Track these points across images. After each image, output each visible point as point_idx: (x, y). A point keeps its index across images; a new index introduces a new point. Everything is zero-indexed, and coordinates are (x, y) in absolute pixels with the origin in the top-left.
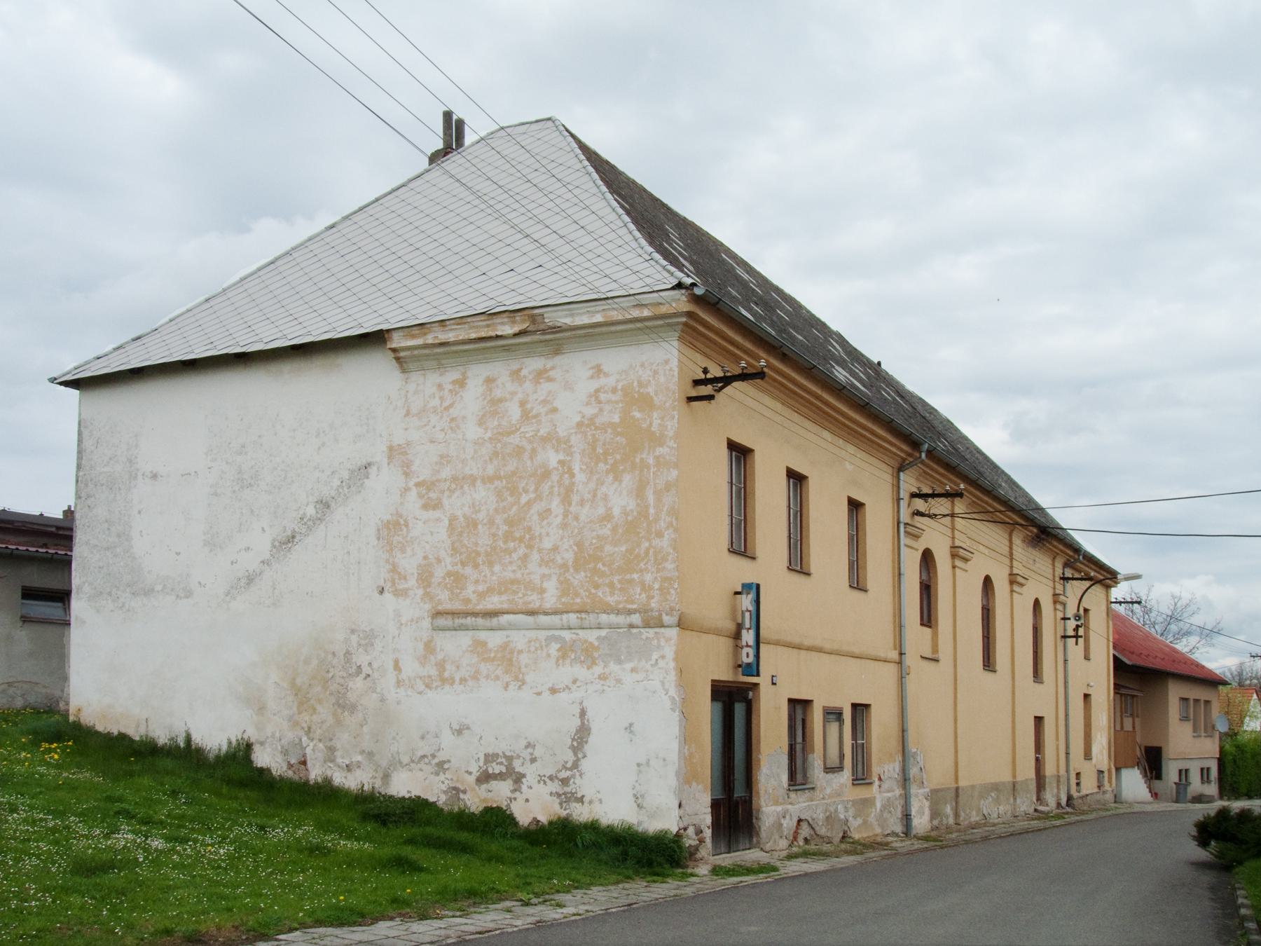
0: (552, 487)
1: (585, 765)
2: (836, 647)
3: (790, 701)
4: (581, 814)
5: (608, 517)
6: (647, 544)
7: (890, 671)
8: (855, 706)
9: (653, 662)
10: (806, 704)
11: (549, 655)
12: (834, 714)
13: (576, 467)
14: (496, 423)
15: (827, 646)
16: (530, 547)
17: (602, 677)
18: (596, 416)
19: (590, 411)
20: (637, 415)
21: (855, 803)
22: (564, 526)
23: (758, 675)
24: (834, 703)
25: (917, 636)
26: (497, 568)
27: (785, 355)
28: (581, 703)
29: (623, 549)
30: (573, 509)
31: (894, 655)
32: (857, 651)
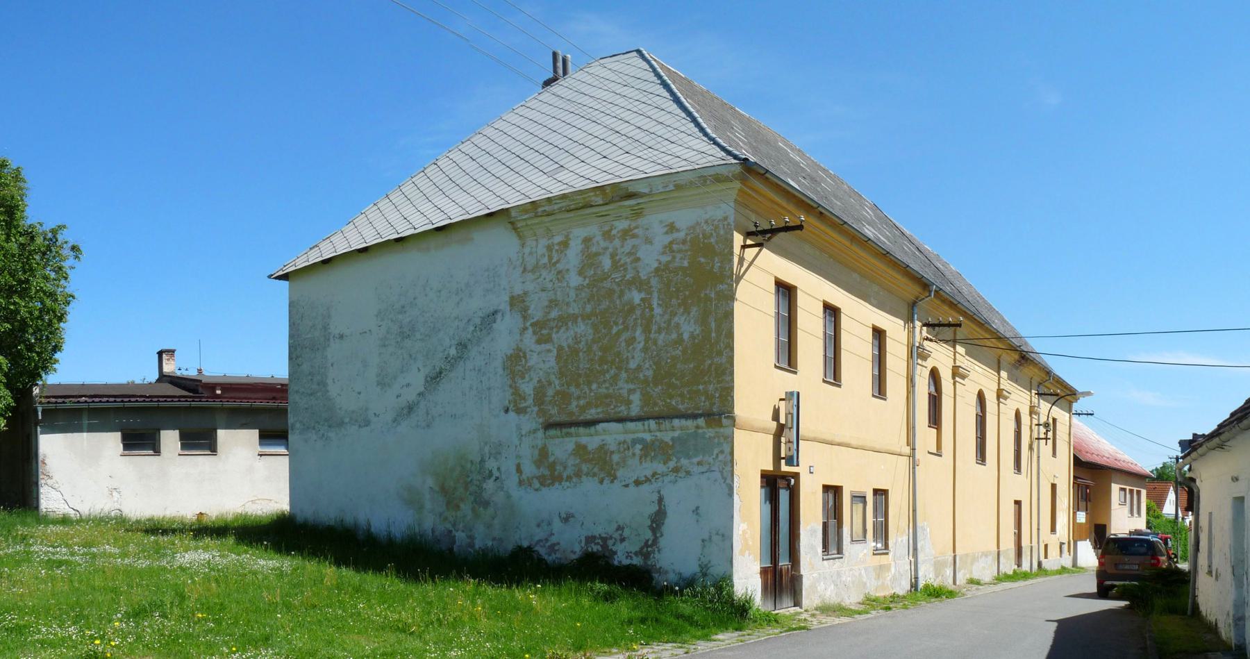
1: (662, 542)
2: (861, 443)
11: (634, 454)
13: (655, 303)
15: (854, 443)
17: (676, 470)
18: (669, 262)
25: (926, 436)
26: (594, 386)
31: (907, 450)
32: (878, 447)
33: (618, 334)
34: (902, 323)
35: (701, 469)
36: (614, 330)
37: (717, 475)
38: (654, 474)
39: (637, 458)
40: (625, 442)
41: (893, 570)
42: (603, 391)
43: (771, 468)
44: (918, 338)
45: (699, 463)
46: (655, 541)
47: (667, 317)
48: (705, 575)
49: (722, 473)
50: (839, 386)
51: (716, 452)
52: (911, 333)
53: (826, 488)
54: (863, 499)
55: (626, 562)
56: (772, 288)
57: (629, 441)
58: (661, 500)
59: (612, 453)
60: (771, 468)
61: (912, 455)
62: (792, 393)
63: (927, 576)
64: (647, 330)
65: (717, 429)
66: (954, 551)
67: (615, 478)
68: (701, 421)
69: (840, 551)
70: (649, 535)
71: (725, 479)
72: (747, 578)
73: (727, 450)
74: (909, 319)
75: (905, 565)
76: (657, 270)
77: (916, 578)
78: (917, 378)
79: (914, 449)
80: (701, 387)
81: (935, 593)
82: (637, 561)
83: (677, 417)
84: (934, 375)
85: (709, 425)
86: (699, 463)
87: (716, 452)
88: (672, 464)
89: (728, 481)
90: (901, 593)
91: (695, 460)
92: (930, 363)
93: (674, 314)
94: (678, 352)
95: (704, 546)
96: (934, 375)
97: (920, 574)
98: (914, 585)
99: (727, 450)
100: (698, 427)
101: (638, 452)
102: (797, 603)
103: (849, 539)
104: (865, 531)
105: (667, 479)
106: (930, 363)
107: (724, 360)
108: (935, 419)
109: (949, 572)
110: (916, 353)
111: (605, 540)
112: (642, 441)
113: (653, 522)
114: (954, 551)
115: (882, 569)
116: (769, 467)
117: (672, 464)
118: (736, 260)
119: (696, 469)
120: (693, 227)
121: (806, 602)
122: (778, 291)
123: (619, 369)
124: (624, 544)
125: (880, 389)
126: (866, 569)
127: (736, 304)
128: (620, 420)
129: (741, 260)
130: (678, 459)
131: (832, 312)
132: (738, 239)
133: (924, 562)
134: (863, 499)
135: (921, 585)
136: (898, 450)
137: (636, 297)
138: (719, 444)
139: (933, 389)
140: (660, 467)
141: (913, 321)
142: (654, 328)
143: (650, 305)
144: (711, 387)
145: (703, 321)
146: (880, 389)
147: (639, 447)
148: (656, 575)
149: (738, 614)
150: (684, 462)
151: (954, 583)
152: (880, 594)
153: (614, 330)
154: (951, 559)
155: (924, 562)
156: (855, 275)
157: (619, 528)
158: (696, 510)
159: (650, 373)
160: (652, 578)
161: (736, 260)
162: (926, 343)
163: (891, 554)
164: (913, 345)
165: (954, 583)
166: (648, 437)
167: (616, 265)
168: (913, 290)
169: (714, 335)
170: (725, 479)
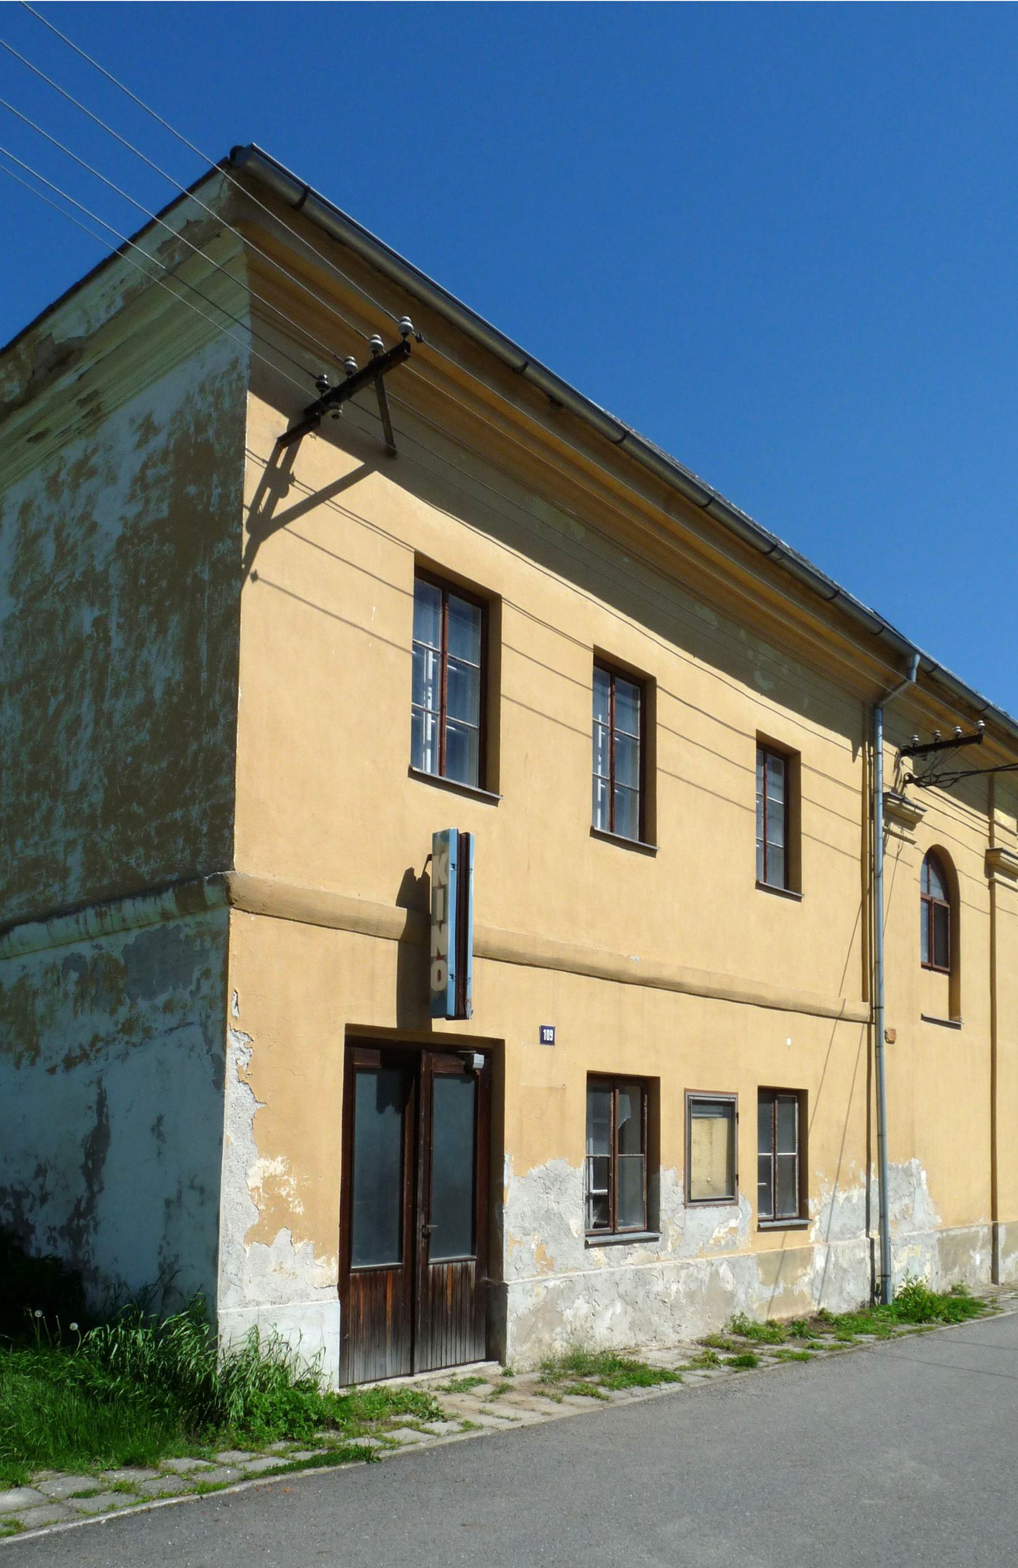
0: (85, 672)
1: (104, 1206)
2: (714, 985)
3: (599, 1083)
4: (336, 1283)
5: (147, 708)
6: (194, 746)
7: (852, 1038)
8: (768, 1095)
9: (193, 987)
10: (646, 1088)
11: (66, 995)
12: (699, 1105)
13: (113, 626)
14: (29, 581)
15: (693, 981)
16: (54, 796)
17: (128, 1028)
18: (139, 516)
19: (132, 511)
20: (192, 490)
21: (762, 1261)
22: (95, 741)
23: (461, 1014)
24: (713, 1083)
25: (911, 985)
26: (19, 843)
27: (555, 403)
28: (99, 1082)
29: (164, 764)
30: (106, 706)
31: (863, 1010)
32: (770, 995)
33: (58, 712)
34: (847, 743)
35: (172, 1020)
36: (53, 704)
37: (197, 1031)
38: (96, 1038)
39: (71, 1003)
40: (53, 967)
41: (819, 1262)
42: (30, 852)
43: (391, 1022)
44: (887, 779)
45: (168, 1007)
46: (91, 1206)
47: (130, 652)
48: (168, 1290)
49: (204, 1026)
50: (652, 853)
51: (196, 974)
52: (872, 766)
53: (599, 1083)
54: (728, 1109)
55: (47, 1250)
56: (407, 580)
57: (60, 963)
58: (101, 1101)
59: (35, 994)
60: (391, 1022)
61: (874, 1020)
62: (445, 836)
63: (916, 1267)
64: (99, 697)
65: (200, 918)
66: (994, 1216)
67: (36, 1051)
68: (168, 900)
69: (652, 1223)
70: (81, 1189)
71: (209, 1042)
72: (279, 1293)
73: (216, 970)
74: (864, 737)
75: (856, 1251)
76: (122, 540)
77: (885, 1276)
78: (887, 863)
79: (879, 1008)
80: (178, 814)
81: (919, 1309)
82: (63, 1249)
83: (132, 895)
84: (938, 861)
85: (185, 909)
86: (168, 1007)
87: (196, 974)
88: (123, 1013)
89: (216, 1049)
90: (837, 1306)
91: (161, 999)
92: (924, 837)
93: (140, 643)
94: (144, 736)
95: (168, 1218)
96: (938, 861)
97: (897, 1266)
98: (879, 1289)
99: (216, 970)
100: (165, 916)
101: (72, 988)
102: (495, 1353)
103: (680, 1197)
104: (732, 1178)
105: (114, 1049)
106: (924, 837)
107: (220, 735)
108: (942, 948)
109: (980, 1258)
110: (886, 812)
111: (19, 1196)
112: (74, 962)
113: (88, 1155)
114: (994, 1216)
115: (782, 1263)
116: (382, 1013)
117: (123, 1013)
118: (253, 474)
119: (161, 1022)
120: (180, 413)
121: (521, 1349)
122: (420, 596)
123: (54, 796)
124: (48, 1207)
125: (782, 869)
126: (733, 1265)
127: (249, 591)
128: (45, 916)
129: (278, 479)
130: (133, 1000)
131: (621, 682)
132: (263, 423)
133: (906, 1241)
134: (728, 1109)
135: (898, 1285)
136: (835, 1008)
137: (86, 616)
138: (204, 953)
139: (937, 894)
140: (103, 1023)
141: (873, 742)
142: (110, 683)
143: (106, 630)
144: (195, 811)
145: (188, 648)
146: (782, 869)
147: (74, 976)
148: (88, 1286)
149: (181, 1395)
150: (143, 1004)
151: (994, 1278)
152: (781, 1315)
153: (53, 704)
154: (985, 1232)
155: (906, 1241)
156: (705, 613)
157: (41, 1172)
158: (157, 1128)
159: (97, 797)
160: (82, 1293)
161: (253, 474)
162: (912, 792)
163: (813, 1232)
164: (874, 792)
165: (994, 1278)
166: (85, 950)
167: (63, 553)
168: (868, 668)
169: (204, 675)
170: (209, 1042)
